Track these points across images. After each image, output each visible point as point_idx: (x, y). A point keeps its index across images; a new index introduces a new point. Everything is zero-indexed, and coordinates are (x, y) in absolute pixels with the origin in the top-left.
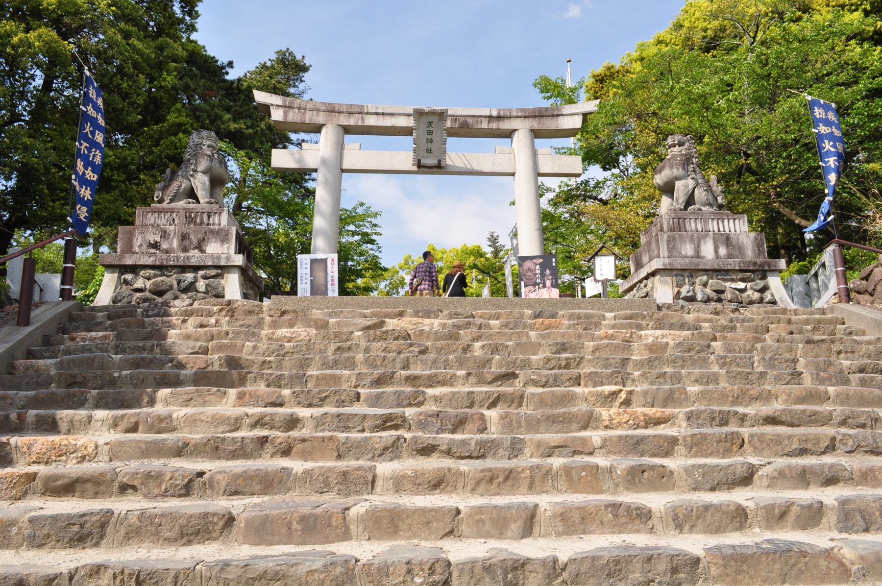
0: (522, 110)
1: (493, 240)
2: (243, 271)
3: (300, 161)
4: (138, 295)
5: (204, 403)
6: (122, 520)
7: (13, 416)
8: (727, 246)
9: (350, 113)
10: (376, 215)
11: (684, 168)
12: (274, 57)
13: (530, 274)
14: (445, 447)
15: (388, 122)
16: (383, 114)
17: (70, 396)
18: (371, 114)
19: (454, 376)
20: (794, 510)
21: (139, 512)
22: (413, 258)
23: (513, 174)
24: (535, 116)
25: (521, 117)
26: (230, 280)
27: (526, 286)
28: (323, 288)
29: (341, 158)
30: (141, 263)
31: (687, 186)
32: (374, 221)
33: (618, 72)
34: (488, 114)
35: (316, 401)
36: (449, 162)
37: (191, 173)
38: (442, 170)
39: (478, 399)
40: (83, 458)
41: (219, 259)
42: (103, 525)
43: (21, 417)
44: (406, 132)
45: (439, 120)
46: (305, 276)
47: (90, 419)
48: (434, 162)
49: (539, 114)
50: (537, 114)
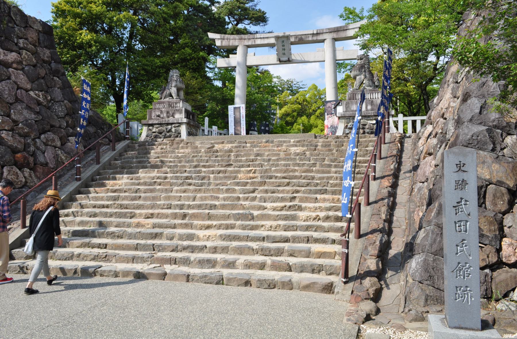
0: (329, 29)
2: (188, 124)
4: (154, 134)
5: (150, 173)
6: (122, 197)
7: (107, 176)
8: (372, 105)
11: (359, 71)
13: (329, 109)
14: (193, 184)
16: (263, 38)
17: (120, 171)
19: (215, 165)
20: (250, 198)
21: (507, 298)
24: (335, 31)
25: (328, 32)
27: (327, 115)
28: (239, 120)
29: (246, 60)
30: (154, 123)
31: (360, 78)
35: (175, 172)
39: (215, 172)
40: (120, 186)
42: (118, 198)
43: (109, 177)
44: (272, 46)
47: (123, 177)
48: (286, 59)
49: (337, 30)
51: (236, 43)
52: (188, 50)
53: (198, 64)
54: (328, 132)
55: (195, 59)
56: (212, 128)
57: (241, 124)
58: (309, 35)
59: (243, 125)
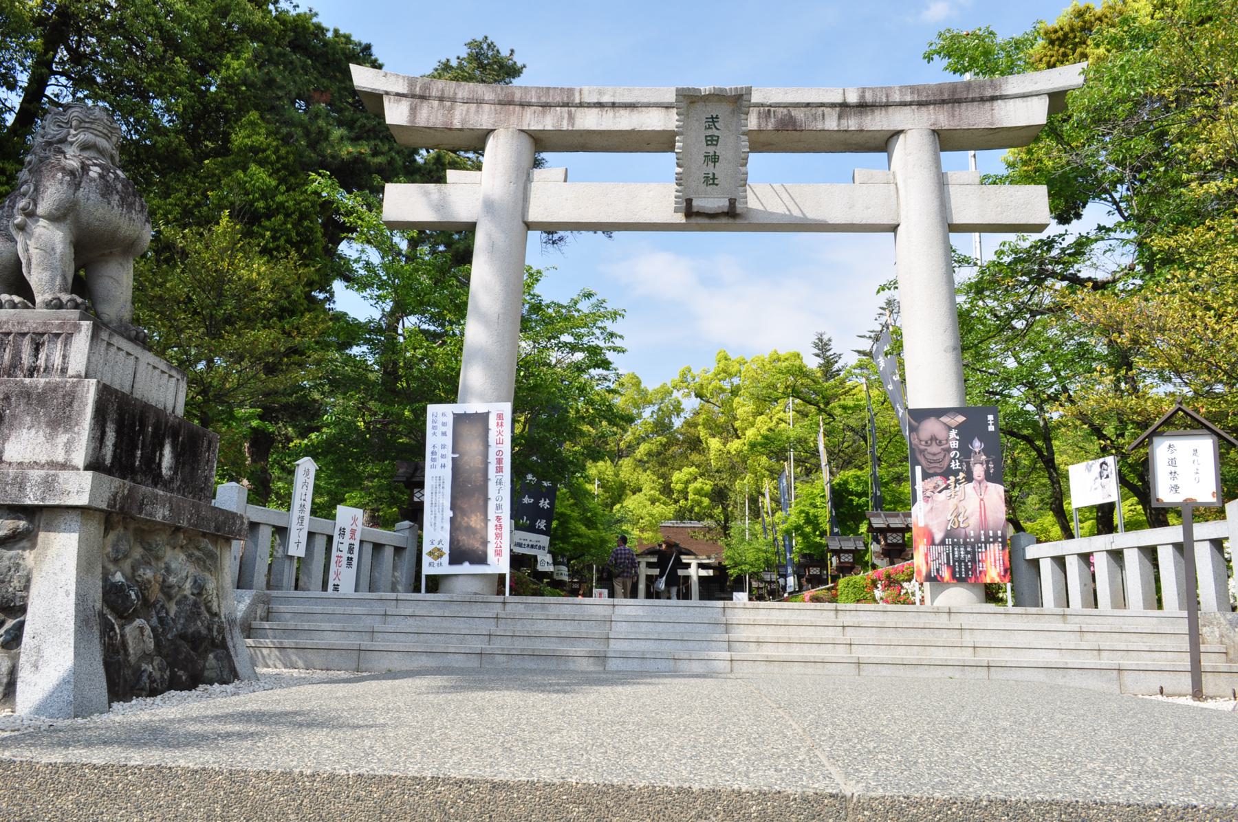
0: (914, 89)
1: (822, 346)
3: (441, 206)
9: (546, 106)
10: (615, 315)
12: (464, 52)
13: (934, 449)
15: (624, 122)
16: (613, 105)
18: (589, 105)
22: (695, 372)
23: (894, 228)
24: (943, 102)
25: (911, 104)
26: (51, 552)
27: (926, 476)
32: (610, 326)
33: (1100, 19)
34: (838, 99)
36: (752, 203)
37: (19, 219)
38: (738, 221)
41: (22, 488)
44: (661, 142)
45: (733, 112)
46: (440, 452)
48: (719, 203)
49: (951, 99)
50: (946, 97)
51: (483, 118)
52: (260, 176)
53: (298, 234)
54: (934, 566)
55: (287, 215)
56: (334, 517)
57: (486, 499)
58: (827, 110)
59: (499, 507)
